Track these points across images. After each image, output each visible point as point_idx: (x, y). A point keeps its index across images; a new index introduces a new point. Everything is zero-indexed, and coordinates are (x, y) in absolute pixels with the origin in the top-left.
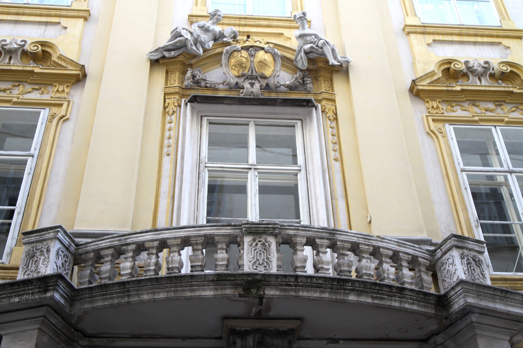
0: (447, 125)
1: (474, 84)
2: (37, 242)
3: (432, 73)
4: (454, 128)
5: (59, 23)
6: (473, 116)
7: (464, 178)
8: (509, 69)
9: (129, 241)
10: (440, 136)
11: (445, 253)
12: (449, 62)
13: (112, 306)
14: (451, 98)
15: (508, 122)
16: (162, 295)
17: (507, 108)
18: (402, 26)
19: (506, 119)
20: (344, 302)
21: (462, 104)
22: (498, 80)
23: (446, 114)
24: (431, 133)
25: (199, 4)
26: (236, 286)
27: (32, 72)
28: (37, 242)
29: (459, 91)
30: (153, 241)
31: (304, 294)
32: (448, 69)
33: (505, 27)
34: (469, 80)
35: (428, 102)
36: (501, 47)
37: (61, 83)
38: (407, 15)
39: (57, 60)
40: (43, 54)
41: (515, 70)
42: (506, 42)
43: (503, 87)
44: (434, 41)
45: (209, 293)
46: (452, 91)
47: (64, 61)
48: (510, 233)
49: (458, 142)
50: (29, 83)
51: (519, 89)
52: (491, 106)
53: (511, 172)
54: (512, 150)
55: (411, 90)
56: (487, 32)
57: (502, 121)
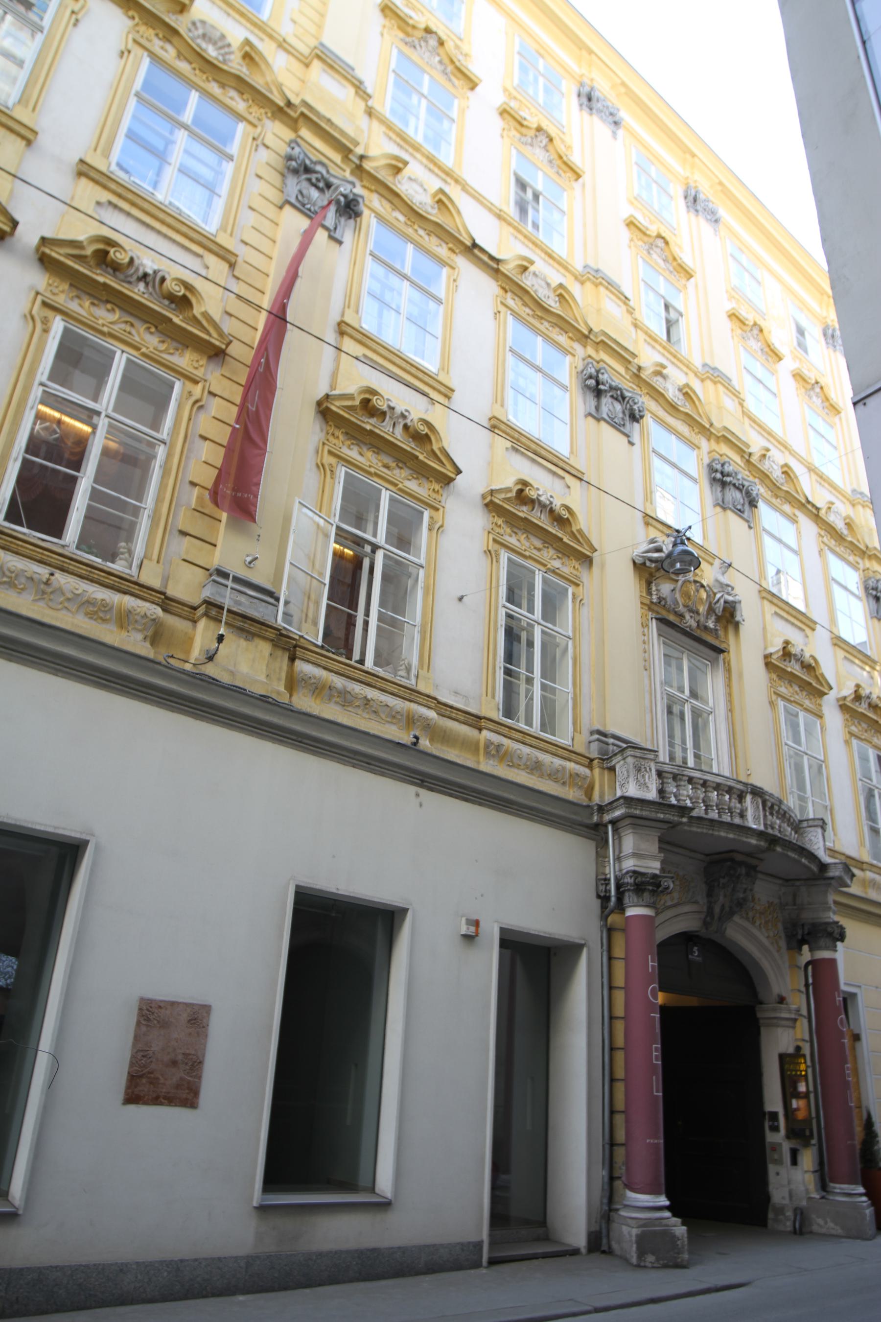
0: (779, 699)
1: (138, 292)
2: (641, 758)
3: (350, 397)
4: (346, 473)
5: (201, 256)
6: (370, 466)
7: (502, 612)
8: (426, 431)
9: (685, 773)
10: (328, 472)
11: (811, 827)
12: (374, 392)
13: (702, 833)
14: (82, 285)
15: (400, 490)
16: (731, 836)
17: (405, 473)
18: (490, 416)
19: (400, 486)
20: (800, 862)
21: (362, 446)
22: (107, 266)
23: (507, 538)
24: (321, 466)
25: (99, 151)
26: (766, 841)
27: (561, 539)
28: (641, 758)
29: (521, 518)
30: (700, 779)
31: (790, 854)
32: (368, 401)
33: (440, 378)
34: (383, 421)
35: (431, 482)
36: (561, 481)
37: (577, 559)
38: (349, 307)
39: (199, 317)
40: (562, 520)
41: (189, 295)
42: (569, 479)
43: (408, 445)
44: (110, 203)
45: (753, 841)
46: (360, 426)
47: (582, 537)
48: (141, 502)
49: (508, 571)
50: (554, 549)
51: (182, 321)
52: (538, 543)
53: (539, 624)
54: (127, 385)
55: (319, 403)
56: (184, 229)
57: (396, 485)
